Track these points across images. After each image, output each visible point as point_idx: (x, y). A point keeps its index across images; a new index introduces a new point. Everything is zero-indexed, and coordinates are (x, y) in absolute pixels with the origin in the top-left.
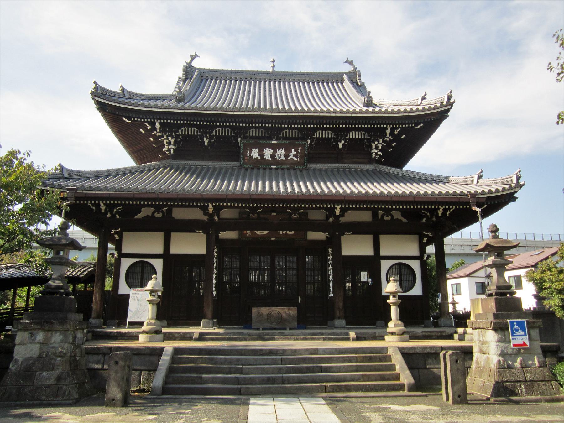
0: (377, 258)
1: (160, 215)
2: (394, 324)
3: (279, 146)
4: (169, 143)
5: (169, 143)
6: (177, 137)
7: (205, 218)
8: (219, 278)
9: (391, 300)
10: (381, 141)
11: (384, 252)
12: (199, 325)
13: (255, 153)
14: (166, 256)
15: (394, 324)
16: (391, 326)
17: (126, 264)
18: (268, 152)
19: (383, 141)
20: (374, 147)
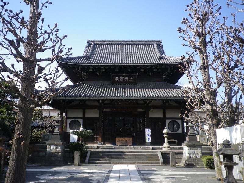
0: (164, 118)
1: (82, 103)
2: (166, 144)
3: (126, 76)
4: (84, 75)
5: (84, 75)
6: (87, 72)
7: (98, 104)
8: (104, 124)
9: (165, 135)
10: (166, 72)
11: (167, 116)
12: (97, 143)
13: (117, 79)
14: (84, 118)
15: (166, 144)
16: (165, 144)
17: (69, 121)
18: (122, 78)
19: (167, 72)
20: (163, 75)
